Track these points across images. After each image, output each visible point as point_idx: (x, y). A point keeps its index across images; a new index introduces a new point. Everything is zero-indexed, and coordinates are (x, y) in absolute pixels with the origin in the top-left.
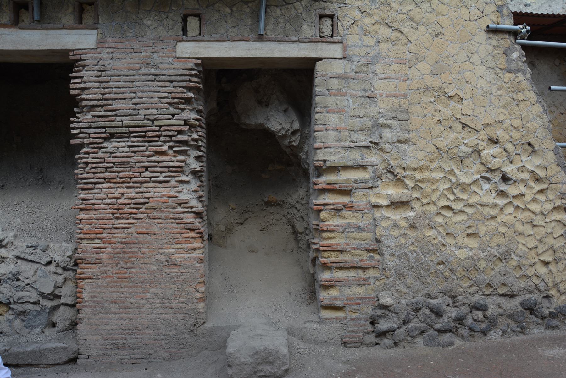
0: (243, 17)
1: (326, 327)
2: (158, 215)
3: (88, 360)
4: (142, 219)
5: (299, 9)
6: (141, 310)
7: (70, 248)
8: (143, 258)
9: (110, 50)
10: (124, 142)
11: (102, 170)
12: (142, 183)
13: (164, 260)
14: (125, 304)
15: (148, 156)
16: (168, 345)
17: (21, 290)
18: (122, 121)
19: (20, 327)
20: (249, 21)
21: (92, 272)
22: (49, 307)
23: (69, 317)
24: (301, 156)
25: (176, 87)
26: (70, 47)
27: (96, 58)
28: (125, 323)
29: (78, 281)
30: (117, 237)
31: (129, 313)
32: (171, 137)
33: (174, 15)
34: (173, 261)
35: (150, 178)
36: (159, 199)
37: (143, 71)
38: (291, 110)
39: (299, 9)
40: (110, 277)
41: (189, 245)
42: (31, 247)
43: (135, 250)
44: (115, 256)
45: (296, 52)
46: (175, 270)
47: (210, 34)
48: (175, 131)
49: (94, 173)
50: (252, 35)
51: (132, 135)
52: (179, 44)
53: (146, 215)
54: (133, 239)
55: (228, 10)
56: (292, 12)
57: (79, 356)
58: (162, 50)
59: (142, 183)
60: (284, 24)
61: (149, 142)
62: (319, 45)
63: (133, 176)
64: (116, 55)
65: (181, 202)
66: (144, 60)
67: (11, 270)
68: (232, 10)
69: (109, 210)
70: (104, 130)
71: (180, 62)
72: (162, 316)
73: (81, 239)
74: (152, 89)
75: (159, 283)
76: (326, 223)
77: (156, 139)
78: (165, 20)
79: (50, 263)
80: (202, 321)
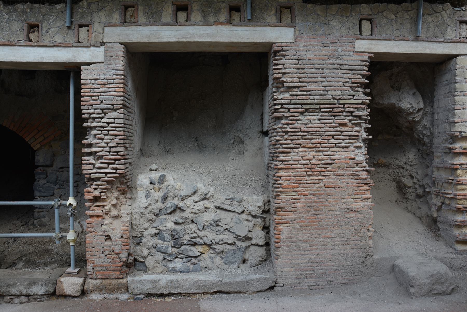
0: (404, 22)
1: (460, 256)
2: (342, 172)
3: (283, 288)
4: (329, 176)
5: (445, 17)
6: (327, 247)
7: (260, 200)
8: (329, 206)
9: (306, 44)
10: (315, 116)
11: (299, 138)
12: (329, 148)
13: (345, 207)
14: (315, 243)
15: (334, 127)
16: (346, 274)
17: (221, 234)
18: (314, 99)
19: (220, 263)
20: (409, 26)
21: (290, 218)
22: (244, 247)
23: (260, 254)
24: (417, 129)
25: (355, 74)
26: (273, 41)
27: (294, 50)
28: (313, 257)
29: (277, 225)
30: (309, 190)
31: (317, 249)
32: (351, 112)
33: (353, 19)
34: (352, 208)
35: (336, 144)
36: (343, 160)
37: (330, 61)
38: (418, 93)
39: (445, 17)
40: (303, 221)
41: (364, 196)
42: (229, 199)
43: (324, 200)
44: (307, 205)
45: (442, 50)
46: (353, 215)
47: (380, 35)
48: (355, 108)
49: (292, 140)
50: (410, 36)
51: (322, 110)
52: (357, 41)
53: (332, 173)
54: (322, 192)
55: (393, 17)
56: (440, 19)
57: (276, 285)
58: (345, 46)
59: (329, 148)
60: (433, 29)
61: (334, 116)
62: (458, 45)
63: (323, 143)
64: (310, 47)
65: (359, 162)
66: (331, 53)
67: (212, 217)
68: (396, 17)
69: (304, 169)
70: (300, 106)
71: (359, 55)
72: (342, 251)
73: (281, 192)
74: (338, 75)
75: (341, 226)
76: (461, 178)
77: (341, 114)
78: (346, 23)
79: (243, 212)
80: (372, 254)
